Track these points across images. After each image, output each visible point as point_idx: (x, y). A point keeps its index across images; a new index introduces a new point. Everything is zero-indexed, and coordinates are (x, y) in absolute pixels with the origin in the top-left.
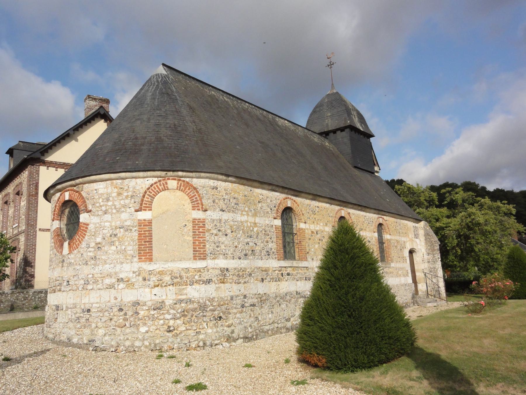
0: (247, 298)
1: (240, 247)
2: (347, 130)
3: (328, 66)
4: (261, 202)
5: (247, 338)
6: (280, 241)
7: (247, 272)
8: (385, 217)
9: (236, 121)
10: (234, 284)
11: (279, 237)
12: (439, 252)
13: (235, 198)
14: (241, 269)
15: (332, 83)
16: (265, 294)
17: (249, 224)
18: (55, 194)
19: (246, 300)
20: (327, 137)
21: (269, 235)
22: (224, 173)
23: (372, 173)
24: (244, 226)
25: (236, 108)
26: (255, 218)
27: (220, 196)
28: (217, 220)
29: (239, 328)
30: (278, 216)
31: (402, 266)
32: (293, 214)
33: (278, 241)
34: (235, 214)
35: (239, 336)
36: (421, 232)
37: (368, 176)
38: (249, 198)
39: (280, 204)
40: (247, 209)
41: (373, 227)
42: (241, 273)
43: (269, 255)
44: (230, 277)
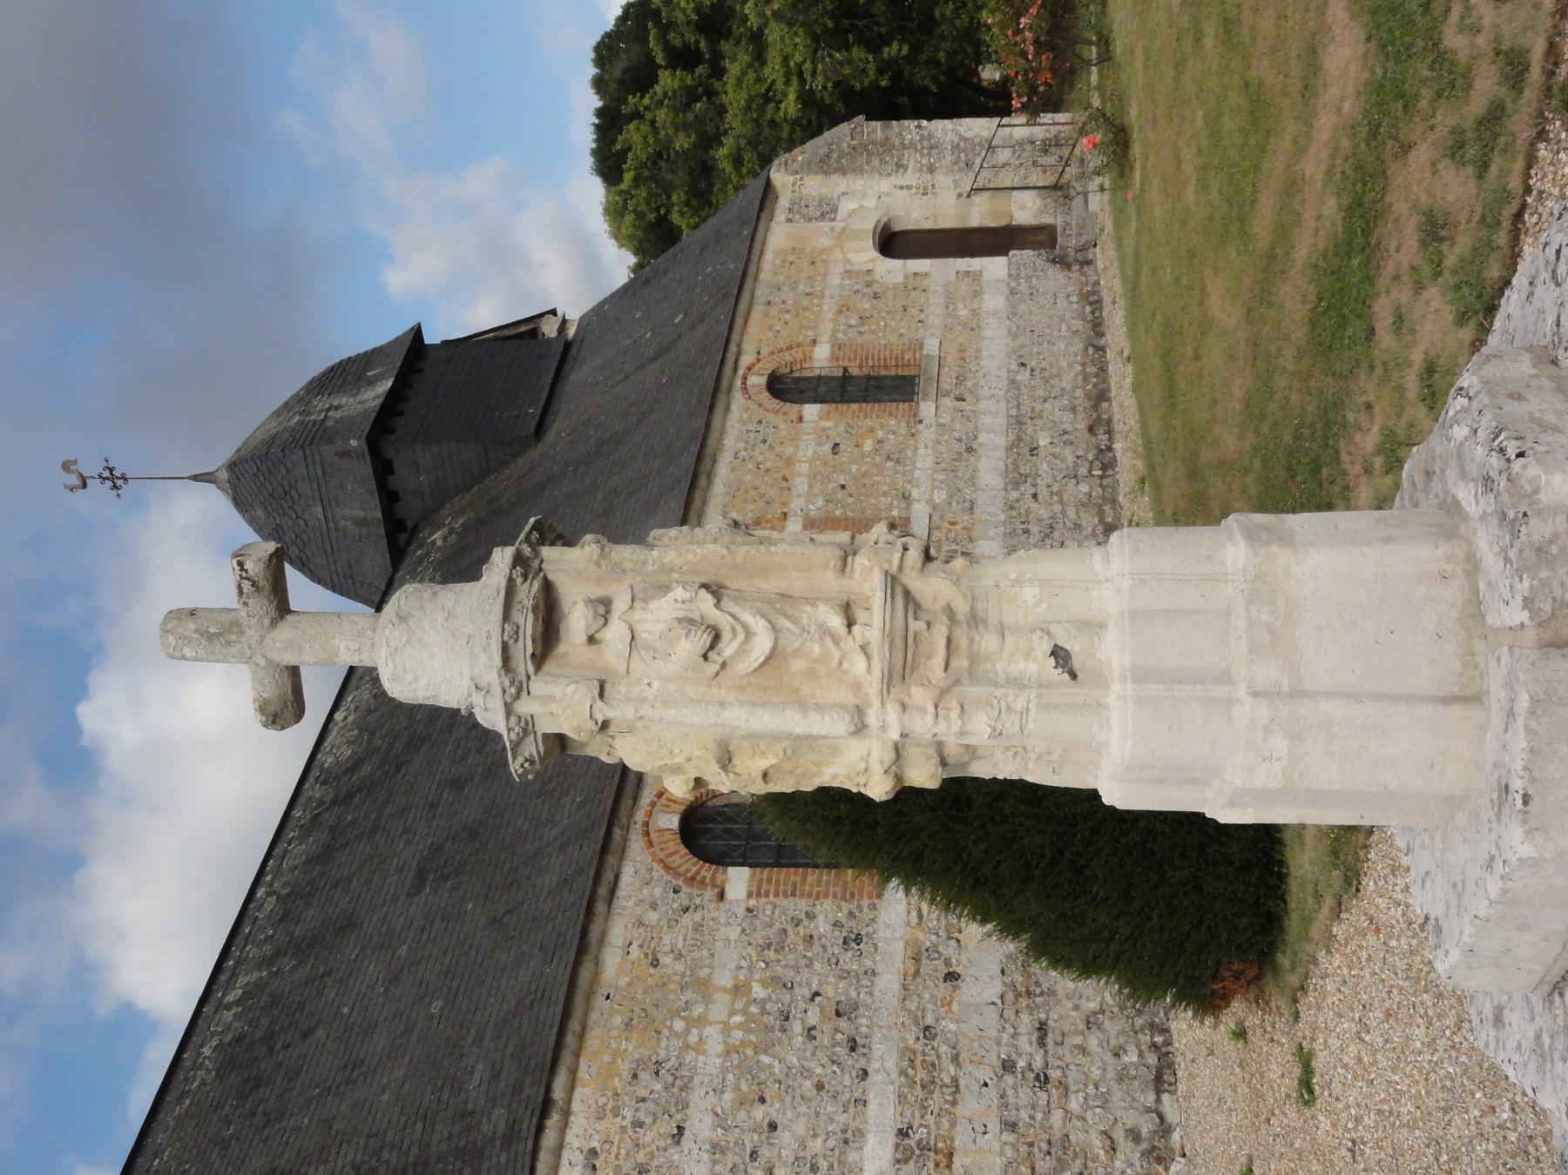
0: (1014, 1056)
1: (819, 1070)
2: (388, 451)
3: (111, 470)
4: (654, 954)
5: (1159, 1078)
6: (810, 879)
7: (918, 1047)
8: (746, 360)
9: (327, 974)
10: (958, 1110)
11: (794, 885)
12: (895, 123)
13: (635, 1076)
14: (903, 1073)
15: (189, 478)
16: (1003, 972)
17: (738, 1019)
18: (563, 1140)
19: (1021, 1063)
20: (410, 525)
21: (785, 931)
22: (535, 1121)
23: (567, 350)
24: (744, 1044)
25: (278, 953)
26: (717, 989)
27: (621, 1140)
28: (715, 1162)
29: (1123, 1104)
30: (713, 879)
31: (941, 300)
32: (710, 804)
33: (807, 888)
34: (697, 1080)
35: (1148, 1110)
36: (814, 185)
37: (577, 376)
38: (637, 1010)
39: (667, 868)
40: (679, 1025)
41: (777, 419)
42: (921, 1075)
43: (858, 939)
44: (933, 1127)
